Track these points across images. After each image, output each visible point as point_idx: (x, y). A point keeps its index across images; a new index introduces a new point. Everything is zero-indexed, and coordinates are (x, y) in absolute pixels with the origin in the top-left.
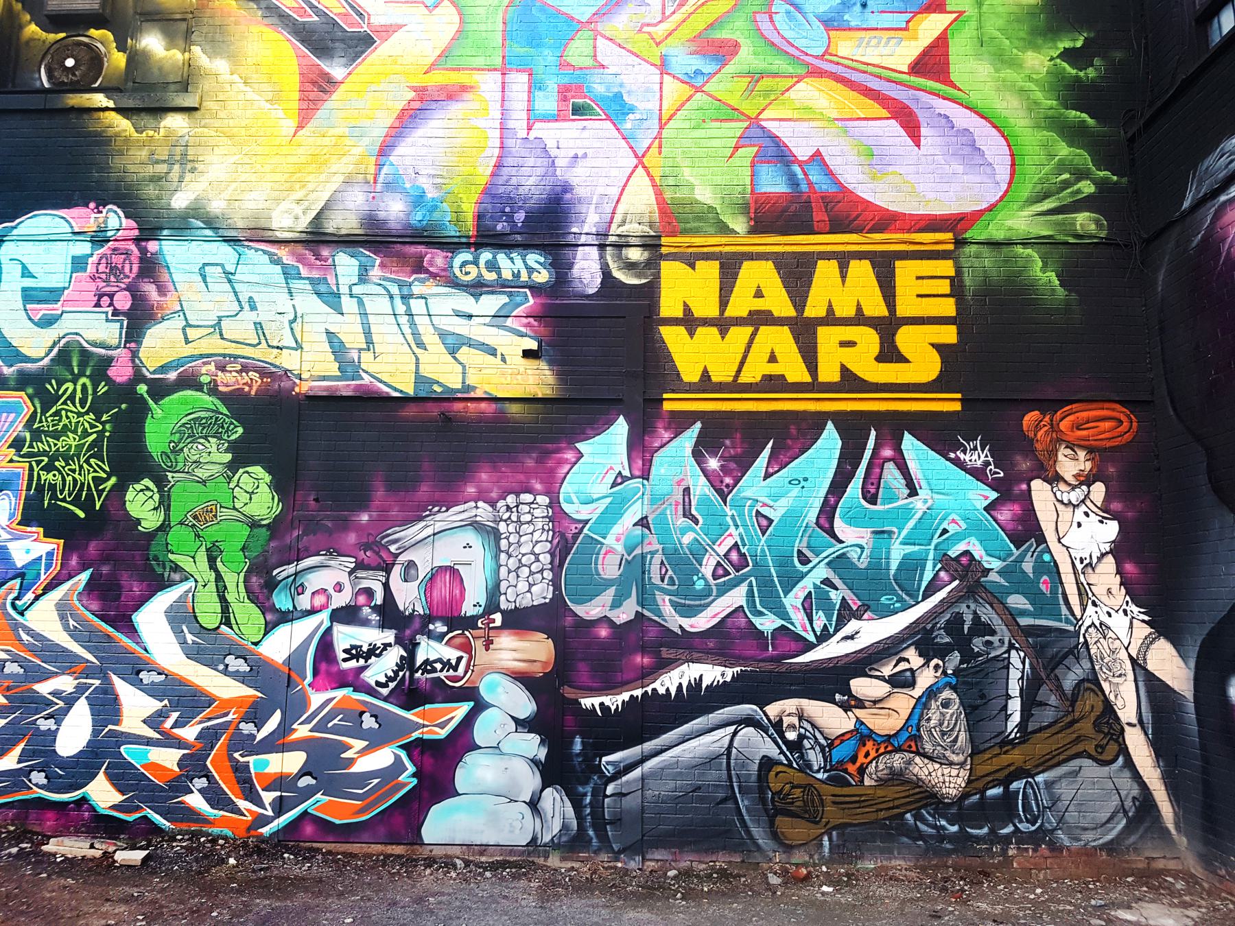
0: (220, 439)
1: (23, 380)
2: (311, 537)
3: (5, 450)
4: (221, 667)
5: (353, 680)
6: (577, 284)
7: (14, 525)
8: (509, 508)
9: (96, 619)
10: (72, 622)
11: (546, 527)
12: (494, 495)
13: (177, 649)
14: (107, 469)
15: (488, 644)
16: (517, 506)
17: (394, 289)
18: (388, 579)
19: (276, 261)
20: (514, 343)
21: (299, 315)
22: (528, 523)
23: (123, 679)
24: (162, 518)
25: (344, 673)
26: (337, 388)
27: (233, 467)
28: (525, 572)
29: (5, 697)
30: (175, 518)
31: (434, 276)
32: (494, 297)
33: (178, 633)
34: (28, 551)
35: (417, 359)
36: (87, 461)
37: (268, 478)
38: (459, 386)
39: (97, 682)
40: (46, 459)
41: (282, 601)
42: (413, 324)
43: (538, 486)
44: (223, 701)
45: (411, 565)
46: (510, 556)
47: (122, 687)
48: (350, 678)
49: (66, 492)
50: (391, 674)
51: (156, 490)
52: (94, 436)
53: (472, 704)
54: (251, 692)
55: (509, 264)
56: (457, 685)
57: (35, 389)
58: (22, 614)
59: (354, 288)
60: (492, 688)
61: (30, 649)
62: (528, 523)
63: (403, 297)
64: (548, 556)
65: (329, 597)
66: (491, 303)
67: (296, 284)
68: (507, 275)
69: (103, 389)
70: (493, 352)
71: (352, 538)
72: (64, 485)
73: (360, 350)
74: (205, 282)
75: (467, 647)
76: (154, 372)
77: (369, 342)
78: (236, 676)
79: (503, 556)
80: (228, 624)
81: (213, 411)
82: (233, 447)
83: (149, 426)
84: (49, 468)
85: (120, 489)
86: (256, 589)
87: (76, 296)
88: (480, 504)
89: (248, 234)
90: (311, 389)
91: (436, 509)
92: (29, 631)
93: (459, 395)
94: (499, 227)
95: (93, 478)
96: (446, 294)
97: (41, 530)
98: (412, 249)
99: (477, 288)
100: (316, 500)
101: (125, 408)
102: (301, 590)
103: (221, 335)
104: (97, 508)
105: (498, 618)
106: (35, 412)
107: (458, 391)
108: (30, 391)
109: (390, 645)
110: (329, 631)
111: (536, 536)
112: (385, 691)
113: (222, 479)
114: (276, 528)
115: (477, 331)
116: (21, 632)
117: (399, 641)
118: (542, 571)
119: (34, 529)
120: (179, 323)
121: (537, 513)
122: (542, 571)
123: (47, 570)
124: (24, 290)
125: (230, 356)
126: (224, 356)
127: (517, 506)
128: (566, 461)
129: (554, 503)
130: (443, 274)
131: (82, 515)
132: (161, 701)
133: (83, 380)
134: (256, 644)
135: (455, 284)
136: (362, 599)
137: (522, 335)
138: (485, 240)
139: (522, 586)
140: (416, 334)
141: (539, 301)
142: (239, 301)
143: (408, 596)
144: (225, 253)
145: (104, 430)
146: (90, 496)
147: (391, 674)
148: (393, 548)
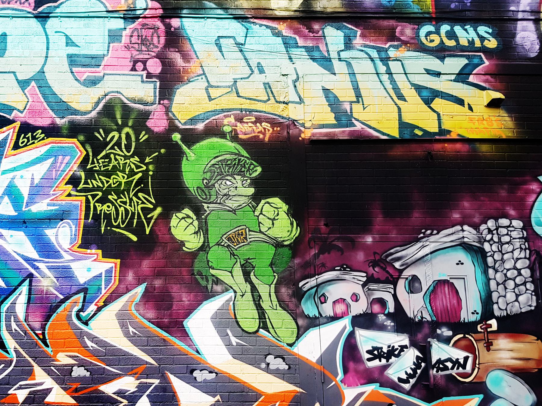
0: (244, 176)
1: (74, 130)
2: (326, 255)
3: (63, 186)
4: (263, 366)
5: (377, 377)
6: (520, 50)
7: (75, 248)
8: (490, 231)
9: (152, 326)
10: (131, 329)
11: (523, 247)
12: (476, 220)
13: (224, 350)
14: (153, 201)
15: (489, 346)
16: (497, 229)
17: (374, 54)
18: (395, 291)
19: (277, 34)
20: (480, 99)
21: (300, 76)
22: (507, 243)
23: (177, 377)
24: (202, 240)
25: (369, 371)
26: (334, 134)
27: (257, 198)
28: (511, 284)
29: (73, 398)
30: (213, 240)
31: (405, 43)
32: (456, 59)
33: (224, 336)
34: (89, 270)
35: (399, 109)
36: (136, 195)
37: (285, 207)
38: (437, 130)
39: (156, 382)
40: (100, 194)
41: (309, 308)
42: (393, 81)
43: (512, 212)
44: (267, 395)
45: (415, 279)
46: (496, 271)
47: (177, 383)
48: (376, 375)
49: (120, 220)
50: (410, 371)
51: (195, 218)
52: (140, 175)
53: (481, 396)
54: (291, 387)
55: (465, 34)
56: (468, 380)
57: (85, 136)
58: (86, 323)
59: (341, 53)
60: (498, 382)
61: (94, 353)
62: (507, 243)
63: (382, 60)
64: (528, 271)
65: (348, 306)
66: (455, 64)
67: (294, 52)
68: (464, 42)
69: (144, 137)
70: (461, 102)
71: (360, 256)
72: (117, 214)
73: (351, 103)
74: (221, 51)
75: (470, 348)
76: (185, 124)
77: (358, 95)
78: (277, 373)
79: (491, 271)
80: (266, 328)
81: (236, 154)
82: (255, 182)
83: (185, 166)
84: (103, 200)
85: (166, 217)
86: (286, 298)
87: (114, 62)
88: (466, 227)
89: (253, 12)
90: (313, 135)
91: (429, 232)
92: (93, 339)
93: (437, 137)
94: (453, 6)
95: (142, 208)
96: (417, 58)
97: (100, 252)
98: (385, 23)
99: (441, 52)
100: (326, 225)
101: (164, 153)
102: (323, 299)
103: (237, 93)
104: (147, 233)
105: (494, 323)
106: (87, 155)
107: (435, 134)
108: (82, 138)
109: (406, 347)
110: (352, 335)
111: (516, 254)
112: (407, 386)
113: (248, 208)
114: (296, 247)
115: (443, 85)
116: (86, 340)
117: (413, 344)
118: (524, 284)
119: (93, 251)
120: (201, 84)
121: (514, 234)
122: (524, 284)
123: (107, 285)
124: (70, 56)
125: (246, 110)
126: (241, 110)
127: (497, 229)
128: (533, 191)
129: (527, 226)
130: (412, 41)
131: (135, 239)
132: (214, 396)
133: (127, 130)
134: (291, 345)
135: (423, 49)
136: (376, 308)
137: (483, 89)
138: (444, 16)
139: (511, 297)
140: (396, 89)
141: (494, 62)
142: (250, 66)
143: (415, 305)
144: (235, 28)
145: (147, 170)
146: (140, 223)
147: (410, 371)
148: (397, 265)
